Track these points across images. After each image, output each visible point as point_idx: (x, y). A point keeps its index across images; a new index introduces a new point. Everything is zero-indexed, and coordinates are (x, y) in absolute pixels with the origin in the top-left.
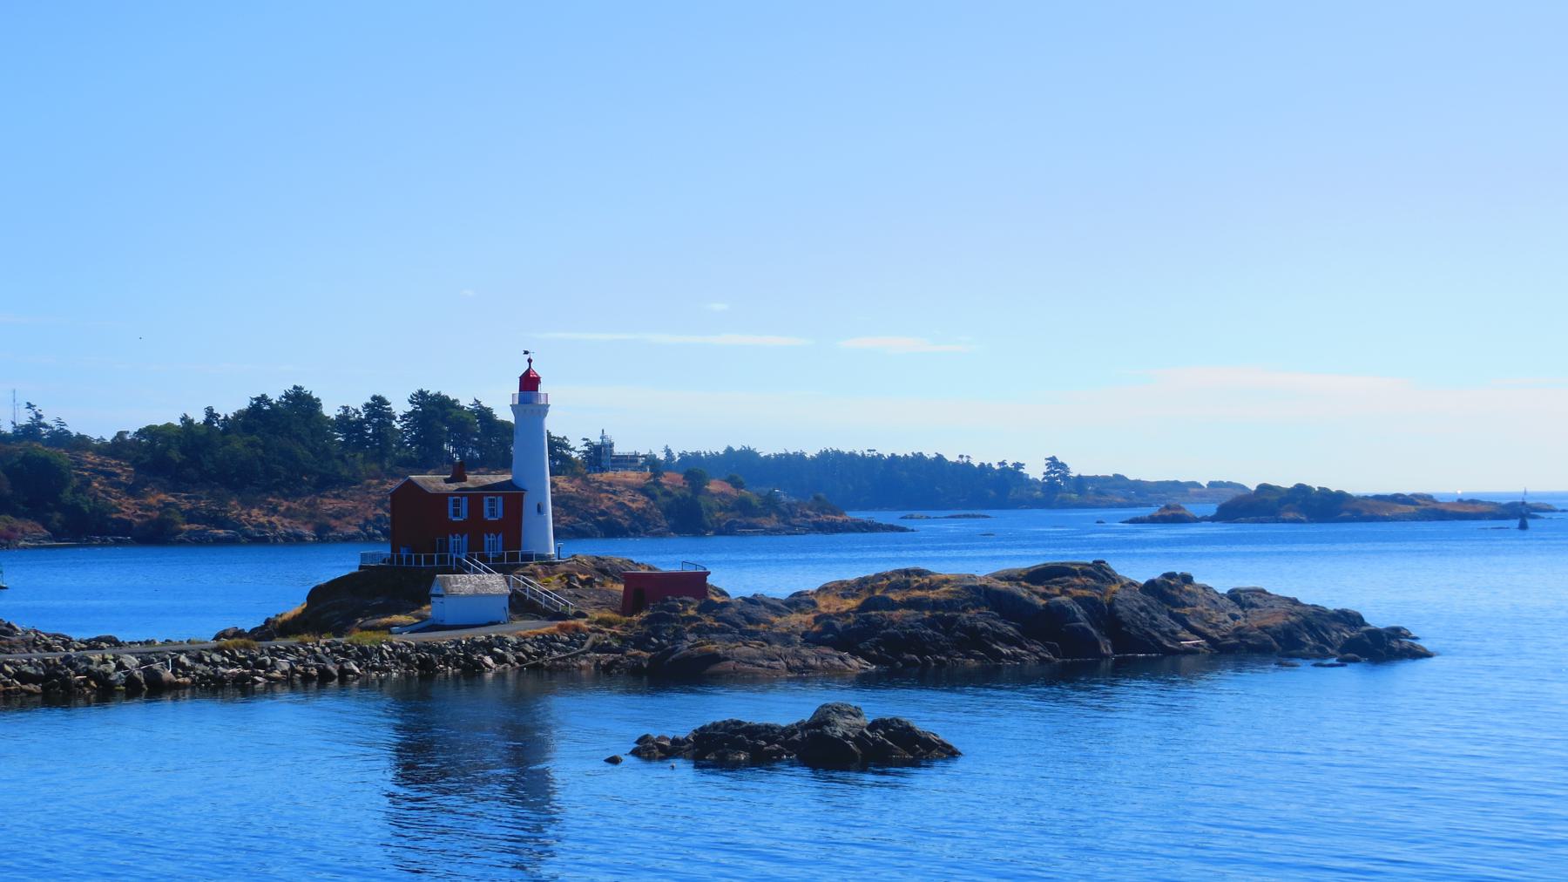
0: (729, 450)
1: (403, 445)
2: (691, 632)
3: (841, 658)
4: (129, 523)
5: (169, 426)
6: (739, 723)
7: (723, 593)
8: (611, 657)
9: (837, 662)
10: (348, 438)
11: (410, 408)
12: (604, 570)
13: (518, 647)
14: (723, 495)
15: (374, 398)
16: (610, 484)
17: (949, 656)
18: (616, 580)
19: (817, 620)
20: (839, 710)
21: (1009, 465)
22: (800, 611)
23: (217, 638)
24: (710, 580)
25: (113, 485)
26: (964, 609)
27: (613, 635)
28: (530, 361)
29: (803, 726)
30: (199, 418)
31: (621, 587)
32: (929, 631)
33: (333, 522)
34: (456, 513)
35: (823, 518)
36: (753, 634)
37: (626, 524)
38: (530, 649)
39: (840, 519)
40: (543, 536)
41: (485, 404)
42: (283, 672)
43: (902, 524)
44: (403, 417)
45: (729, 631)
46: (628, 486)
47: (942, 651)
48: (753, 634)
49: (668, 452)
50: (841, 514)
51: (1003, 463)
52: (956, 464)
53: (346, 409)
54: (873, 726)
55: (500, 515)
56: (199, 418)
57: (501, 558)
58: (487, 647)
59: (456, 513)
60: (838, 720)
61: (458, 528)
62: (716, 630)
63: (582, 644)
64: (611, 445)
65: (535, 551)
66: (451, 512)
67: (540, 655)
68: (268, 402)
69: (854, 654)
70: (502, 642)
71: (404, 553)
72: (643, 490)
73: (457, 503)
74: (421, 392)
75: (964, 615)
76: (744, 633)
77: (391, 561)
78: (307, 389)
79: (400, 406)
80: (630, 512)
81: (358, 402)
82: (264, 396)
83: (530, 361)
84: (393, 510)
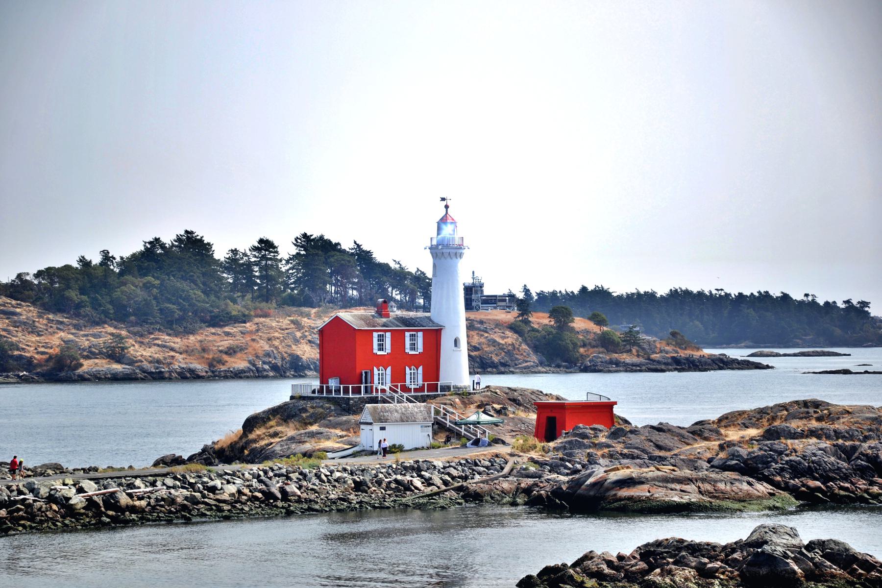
0: (584, 289)
1: (286, 285)
2: (603, 456)
3: (749, 483)
4: (30, 360)
5: (67, 268)
6: (681, 541)
7: (626, 422)
8: (530, 481)
9: (745, 487)
10: (236, 279)
11: (294, 251)
12: (515, 399)
13: (444, 470)
14: (587, 332)
15: (261, 241)
16: (481, 322)
17: (852, 483)
18: (527, 410)
19: (722, 447)
20: (774, 530)
21: (855, 302)
22: (706, 439)
23: (156, 464)
24: (617, 410)
25: (16, 324)
26: (866, 438)
27: (532, 460)
28: (447, 207)
29: (739, 546)
30: (96, 259)
31: (534, 416)
32: (833, 459)
33: (225, 357)
34: (413, 347)
35: (683, 354)
36: (662, 459)
37: (496, 359)
38: (454, 473)
39: (697, 354)
40: (457, 369)
41: (365, 247)
42: (232, 495)
43: (764, 361)
44: (288, 262)
45: (638, 457)
46: (498, 325)
47: (846, 478)
48: (662, 459)
49: (527, 291)
50: (698, 349)
51: (847, 302)
52: (802, 302)
53: (235, 252)
54: (811, 546)
55: (420, 348)
56: (96, 259)
57: (421, 389)
58: (417, 469)
59: (413, 347)
60: (775, 538)
61: (382, 362)
62: (625, 456)
63: (502, 468)
64: (481, 286)
65: (453, 383)
66: (375, 346)
67: (465, 478)
68: (163, 246)
69: (759, 480)
70: (432, 467)
71: (333, 383)
72: (513, 328)
73: (381, 338)
74: (305, 235)
75: (865, 445)
76: (651, 458)
77: (321, 391)
78: (199, 233)
79: (286, 249)
80: (501, 347)
81: (245, 243)
82: (157, 240)
83: (447, 207)
84: (322, 347)
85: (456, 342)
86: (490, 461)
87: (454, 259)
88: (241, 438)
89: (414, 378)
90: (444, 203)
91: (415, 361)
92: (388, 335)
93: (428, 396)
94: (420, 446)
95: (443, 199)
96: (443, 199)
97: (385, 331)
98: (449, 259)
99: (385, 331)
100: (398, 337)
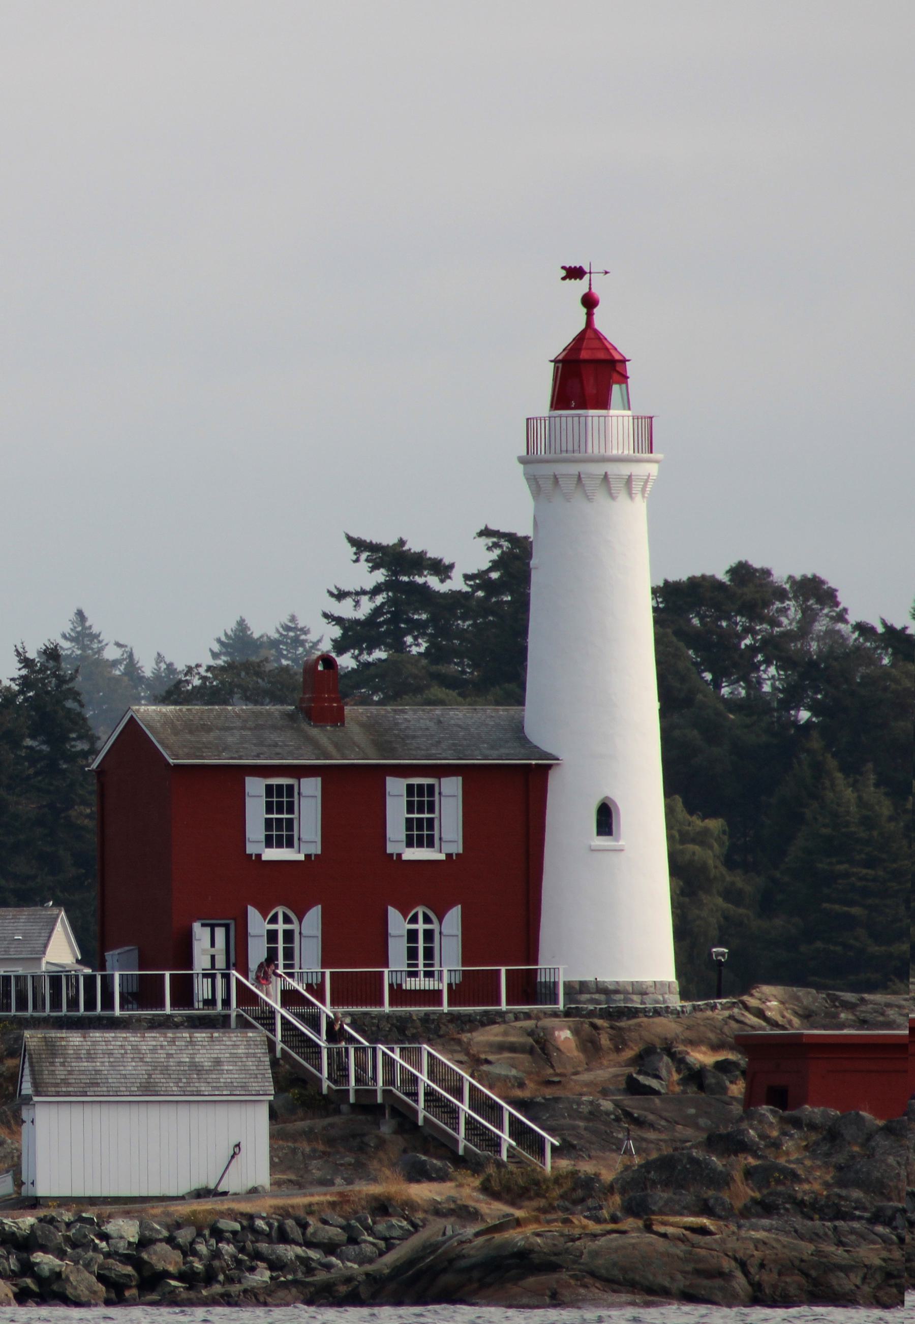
28: (589, 302)
34: (421, 833)
59: (421, 833)
61: (286, 888)
83: (589, 302)
85: (606, 820)
86: (347, 1228)
87: (622, 497)
88: (553, 1046)
89: (422, 949)
90: (579, 287)
91: (427, 888)
92: (311, 787)
93: (453, 1018)
94: (173, 1193)
95: (575, 273)
96: (575, 273)
97: (300, 772)
98: (601, 497)
99: (300, 772)
100: (353, 794)
